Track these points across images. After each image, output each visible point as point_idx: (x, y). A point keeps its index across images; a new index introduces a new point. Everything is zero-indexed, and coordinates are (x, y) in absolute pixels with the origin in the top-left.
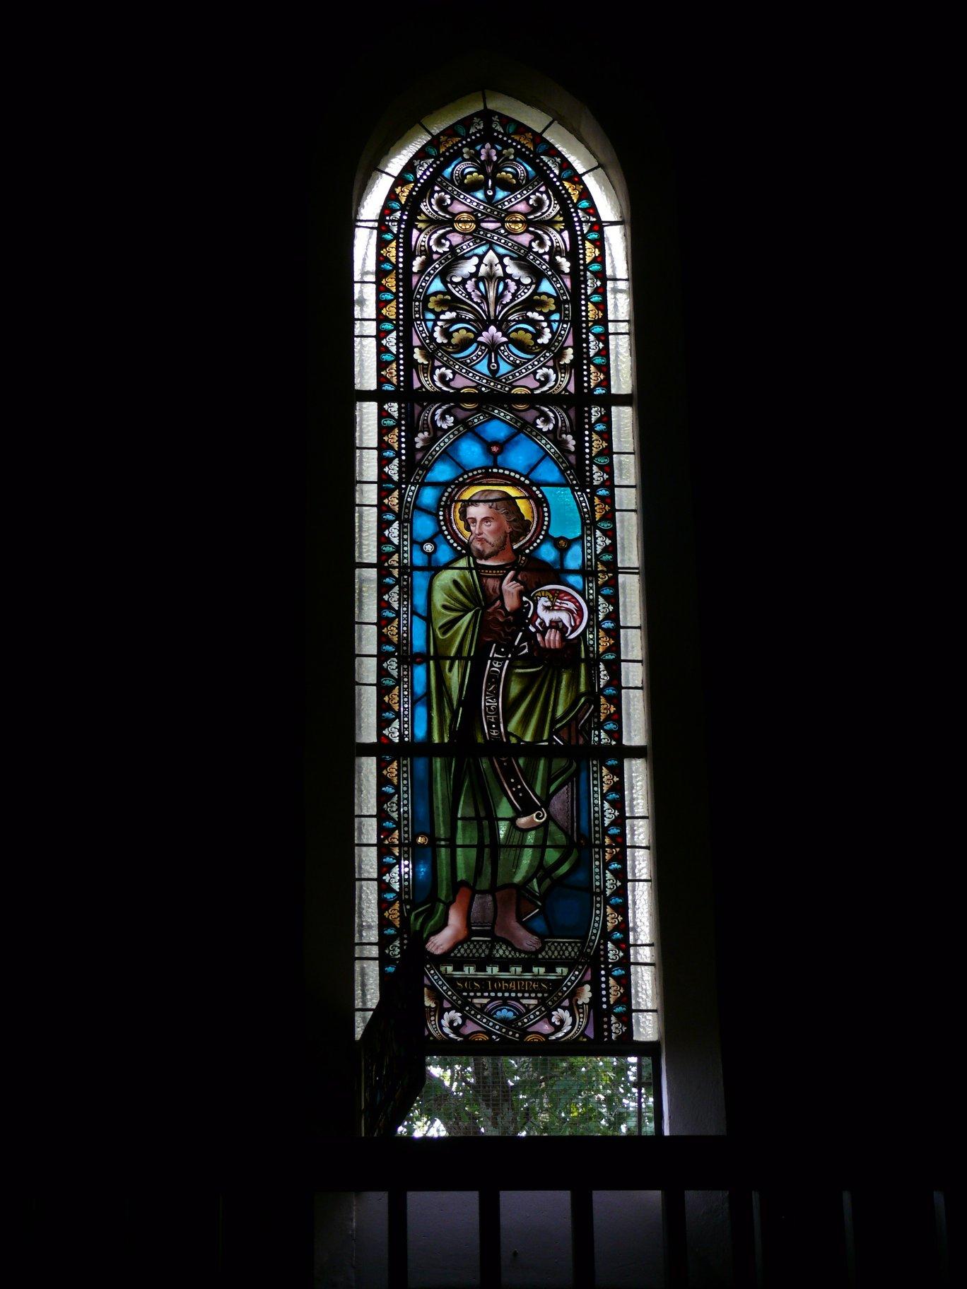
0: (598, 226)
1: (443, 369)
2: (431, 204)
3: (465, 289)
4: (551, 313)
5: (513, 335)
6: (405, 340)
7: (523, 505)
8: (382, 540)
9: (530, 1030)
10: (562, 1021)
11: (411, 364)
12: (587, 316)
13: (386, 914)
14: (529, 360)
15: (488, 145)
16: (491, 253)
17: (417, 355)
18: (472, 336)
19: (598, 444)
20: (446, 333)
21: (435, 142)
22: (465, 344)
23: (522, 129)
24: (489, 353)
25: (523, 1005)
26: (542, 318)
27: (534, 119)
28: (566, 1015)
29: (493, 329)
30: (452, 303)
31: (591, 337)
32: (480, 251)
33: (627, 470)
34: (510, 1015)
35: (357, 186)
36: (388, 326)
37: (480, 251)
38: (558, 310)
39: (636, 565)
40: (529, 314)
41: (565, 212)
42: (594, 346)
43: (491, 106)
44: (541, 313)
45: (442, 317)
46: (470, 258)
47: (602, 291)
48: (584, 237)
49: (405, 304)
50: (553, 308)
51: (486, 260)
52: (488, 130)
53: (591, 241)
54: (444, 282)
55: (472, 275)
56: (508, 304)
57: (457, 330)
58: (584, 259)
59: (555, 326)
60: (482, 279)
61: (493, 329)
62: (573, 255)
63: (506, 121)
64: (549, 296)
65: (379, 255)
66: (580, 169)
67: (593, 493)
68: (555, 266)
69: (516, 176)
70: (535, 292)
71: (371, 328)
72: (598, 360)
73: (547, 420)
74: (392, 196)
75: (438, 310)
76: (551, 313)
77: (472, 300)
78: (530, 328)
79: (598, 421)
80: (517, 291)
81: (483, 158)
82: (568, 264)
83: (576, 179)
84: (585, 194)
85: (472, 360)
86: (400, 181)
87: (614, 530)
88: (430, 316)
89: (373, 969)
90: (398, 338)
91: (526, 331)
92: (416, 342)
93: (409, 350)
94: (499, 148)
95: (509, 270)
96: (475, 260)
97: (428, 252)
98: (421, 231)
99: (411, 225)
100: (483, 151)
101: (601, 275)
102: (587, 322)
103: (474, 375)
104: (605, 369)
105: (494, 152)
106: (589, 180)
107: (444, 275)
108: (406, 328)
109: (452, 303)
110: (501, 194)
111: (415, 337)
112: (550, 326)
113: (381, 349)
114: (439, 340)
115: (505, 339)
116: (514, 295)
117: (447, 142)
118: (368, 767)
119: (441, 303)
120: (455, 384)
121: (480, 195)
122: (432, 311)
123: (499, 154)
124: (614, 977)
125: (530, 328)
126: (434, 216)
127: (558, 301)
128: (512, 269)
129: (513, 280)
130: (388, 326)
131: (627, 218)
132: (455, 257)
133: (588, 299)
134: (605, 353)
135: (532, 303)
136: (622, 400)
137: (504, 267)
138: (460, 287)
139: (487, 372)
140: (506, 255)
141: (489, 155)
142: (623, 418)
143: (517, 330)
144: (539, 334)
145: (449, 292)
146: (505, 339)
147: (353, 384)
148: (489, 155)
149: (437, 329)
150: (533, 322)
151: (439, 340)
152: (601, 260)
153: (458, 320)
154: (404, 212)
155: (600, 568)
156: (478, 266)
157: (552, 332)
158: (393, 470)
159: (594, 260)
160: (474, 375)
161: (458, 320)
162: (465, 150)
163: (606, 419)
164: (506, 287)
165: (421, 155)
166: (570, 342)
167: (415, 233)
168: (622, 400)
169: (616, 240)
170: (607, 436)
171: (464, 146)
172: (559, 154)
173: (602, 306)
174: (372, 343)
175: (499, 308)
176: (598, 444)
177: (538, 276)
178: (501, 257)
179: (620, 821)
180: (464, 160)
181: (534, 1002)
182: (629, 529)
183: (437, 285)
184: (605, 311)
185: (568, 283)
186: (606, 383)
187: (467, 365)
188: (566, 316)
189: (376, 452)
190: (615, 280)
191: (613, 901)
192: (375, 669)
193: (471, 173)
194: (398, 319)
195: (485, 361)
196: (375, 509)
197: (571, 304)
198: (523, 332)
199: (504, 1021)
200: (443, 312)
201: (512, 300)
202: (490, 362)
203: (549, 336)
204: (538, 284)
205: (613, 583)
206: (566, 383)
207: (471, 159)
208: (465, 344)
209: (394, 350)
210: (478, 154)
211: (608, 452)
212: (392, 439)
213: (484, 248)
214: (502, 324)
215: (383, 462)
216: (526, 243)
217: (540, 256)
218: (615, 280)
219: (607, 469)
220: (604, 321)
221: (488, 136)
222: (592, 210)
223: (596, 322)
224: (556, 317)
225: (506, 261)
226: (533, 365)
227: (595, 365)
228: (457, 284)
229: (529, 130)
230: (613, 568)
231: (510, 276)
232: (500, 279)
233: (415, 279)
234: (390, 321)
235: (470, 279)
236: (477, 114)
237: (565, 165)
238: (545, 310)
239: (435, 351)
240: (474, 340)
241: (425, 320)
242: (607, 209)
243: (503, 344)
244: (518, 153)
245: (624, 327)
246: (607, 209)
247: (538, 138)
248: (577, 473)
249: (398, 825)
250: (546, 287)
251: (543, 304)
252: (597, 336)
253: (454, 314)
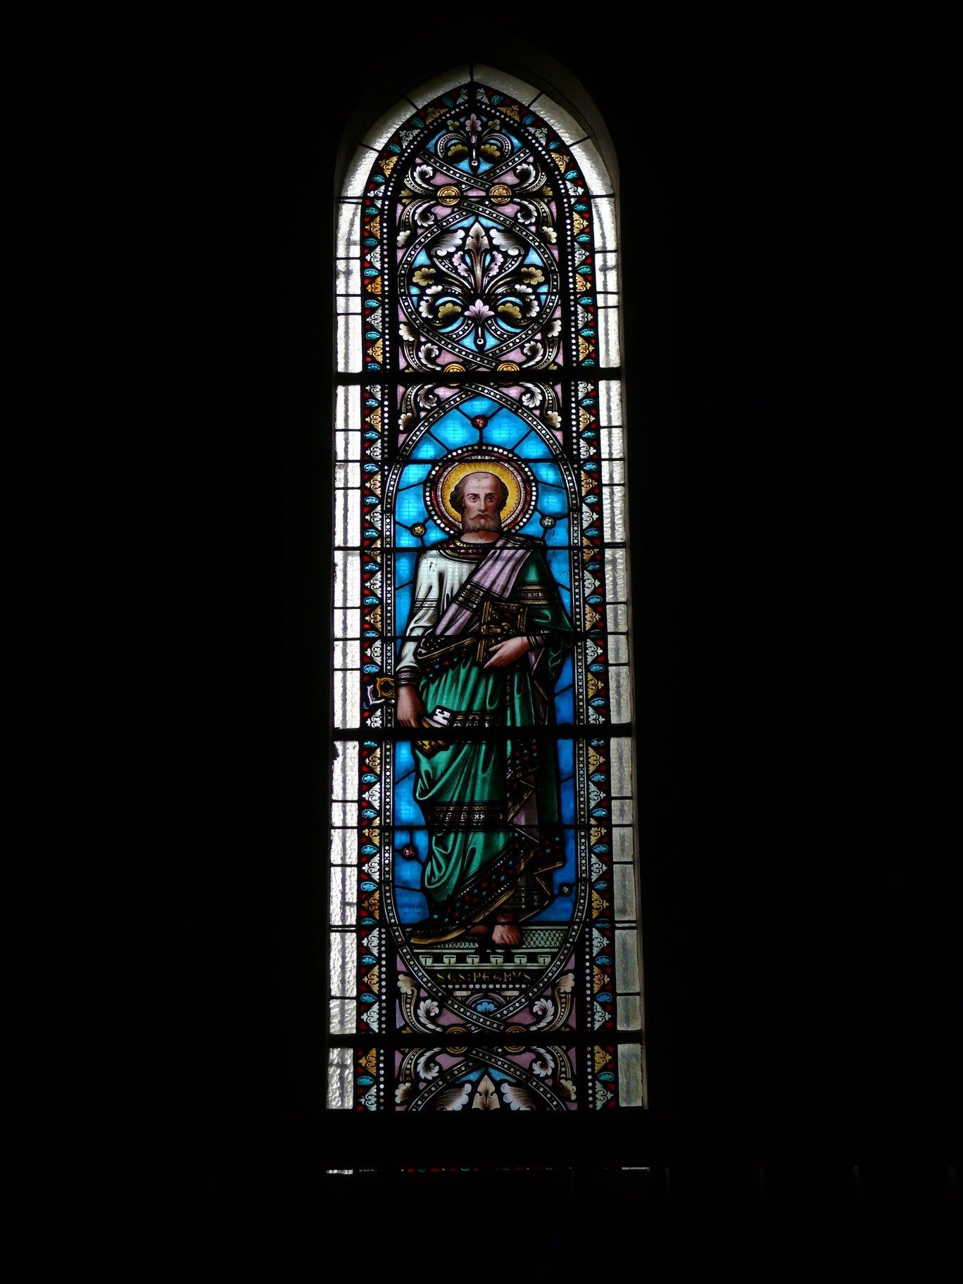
0: (587, 198)
1: (429, 345)
2: (413, 178)
3: (452, 263)
4: (540, 284)
5: (501, 308)
6: (392, 323)
7: (512, 501)
8: (365, 525)
9: (503, 358)
10: (545, 1011)
11: (397, 342)
12: (575, 288)
13: (368, 722)
14: (517, 334)
15: (473, 116)
16: (477, 226)
17: (403, 332)
18: (459, 309)
19: (585, 418)
20: (433, 309)
21: (421, 114)
22: (450, 319)
23: (508, 101)
24: (476, 328)
25: (504, 997)
26: (530, 290)
27: (522, 93)
28: (549, 1004)
29: (479, 303)
30: (439, 278)
31: (580, 309)
32: (466, 223)
33: (613, 443)
34: (492, 1007)
35: (338, 170)
36: (373, 303)
37: (466, 223)
38: (546, 282)
39: (634, 918)
40: (517, 287)
41: (552, 182)
42: (582, 317)
43: (476, 78)
44: (529, 285)
45: (429, 291)
46: (456, 231)
47: (589, 261)
48: (571, 208)
49: (388, 291)
50: (542, 279)
51: (480, 1089)
52: (472, 100)
53: (579, 213)
54: (430, 256)
55: (459, 248)
56: (494, 277)
57: (444, 304)
58: (592, 1067)
59: (543, 297)
60: (468, 252)
61: (479, 303)
62: (559, 226)
63: (490, 92)
64: (537, 267)
65: (363, 588)
66: (568, 141)
67: (580, 468)
68: (544, 238)
69: (500, 149)
70: (522, 265)
71: (356, 305)
72: (603, 960)
73: (544, 1065)
74: (377, 169)
75: (423, 283)
76: (540, 284)
77: (459, 274)
78: (517, 301)
79: (583, 263)
80: (503, 264)
81: (468, 129)
82: (560, 419)
83: (564, 150)
84: (573, 164)
85: (458, 335)
86: (384, 154)
87: (616, 1081)
88: (414, 291)
89: (354, 679)
90: (383, 316)
91: (514, 304)
92: (402, 317)
93: (393, 325)
94: (484, 119)
95: (495, 242)
96: (468, 1088)
97: (413, 227)
98: (405, 206)
99: (395, 200)
100: (468, 123)
101: (589, 246)
102: (575, 294)
103: (455, 173)
104: (593, 340)
105: (479, 123)
106: (577, 151)
107: (430, 248)
108: (392, 300)
109: (439, 278)
110: (485, 167)
111: (400, 312)
112: (538, 299)
113: (367, 327)
114: (424, 315)
115: (492, 313)
116: (501, 267)
117: (433, 113)
118: (349, 753)
119: (425, 277)
120: (442, 1021)
121: (464, 165)
122: (417, 285)
123: (484, 125)
124: (601, 1082)
125: (517, 301)
126: (418, 190)
127: (545, 270)
128: (498, 239)
129: (500, 252)
130: (373, 303)
131: (618, 192)
132: (445, 232)
133: (575, 271)
134: (593, 325)
135: (519, 276)
136: (610, 374)
137: (490, 239)
138: (447, 262)
139: (473, 347)
140: (504, 1081)
141: (473, 126)
142: (611, 395)
143: (504, 304)
144: (526, 308)
145: (433, 265)
146: (492, 313)
147: (329, 920)
148: (473, 126)
149: (423, 303)
150: (522, 296)
151: (424, 315)
152: (589, 230)
153: (443, 294)
154: (390, 181)
155: (593, 822)
156: (471, 1096)
157: (540, 305)
158: (377, 452)
159: (582, 232)
160: (455, 173)
161: (443, 294)
162: (449, 122)
163: (594, 395)
164: (493, 259)
165: (408, 126)
166: (558, 314)
167: (400, 208)
168: (610, 374)
169: (605, 212)
170: (594, 410)
171: (448, 119)
172: (546, 125)
173: (591, 278)
174: (356, 322)
175: (486, 280)
176: (585, 418)
177: (525, 247)
178: (498, 1084)
179: (606, 804)
180: (449, 132)
181: (516, 993)
182: (615, 504)
183: (422, 259)
184: (593, 283)
185: (556, 253)
186: (595, 355)
187: (453, 340)
188: (555, 287)
189: (359, 317)
190: (606, 293)
191: (597, 850)
192: (355, 946)
193: (455, 145)
194: (383, 295)
195: (472, 336)
196: (358, 642)
197: (559, 271)
198: (511, 305)
199: (487, 1013)
200: (429, 286)
201: (498, 274)
202: (476, 337)
203: (538, 309)
204: (525, 256)
205: (599, 558)
206: (555, 357)
207: (456, 130)
208: (450, 319)
209: (378, 265)
210: (463, 126)
211: (595, 427)
212: (375, 419)
213: (471, 220)
214: (490, 300)
215: (366, 444)
216: (512, 215)
217: (526, 227)
218: (606, 293)
219: (612, 1086)
220: (592, 293)
221: (473, 107)
222: (580, 181)
223: (584, 294)
224: (544, 289)
225: (506, 1088)
226: (521, 338)
227: (590, 605)
228: (442, 258)
229: (515, 102)
230: (599, 544)
231: (497, 248)
232: (487, 252)
233: (400, 254)
234: (376, 462)
235: (456, 252)
236: (464, 86)
237: (552, 136)
238: (534, 282)
239: (421, 326)
240: (461, 314)
241: (411, 296)
242: (595, 183)
243: (490, 318)
244: (504, 124)
245: (613, 300)
246: (595, 183)
247: (525, 111)
248: (564, 456)
249: (379, 813)
250: (533, 258)
251: (532, 276)
252: (585, 307)
253: (440, 288)
